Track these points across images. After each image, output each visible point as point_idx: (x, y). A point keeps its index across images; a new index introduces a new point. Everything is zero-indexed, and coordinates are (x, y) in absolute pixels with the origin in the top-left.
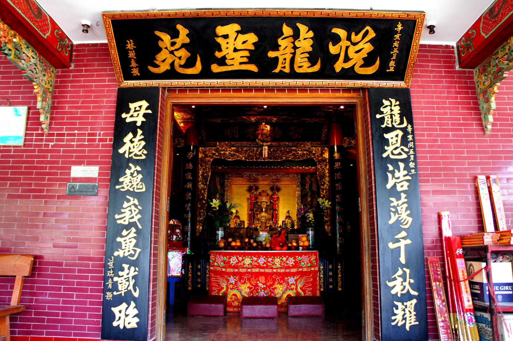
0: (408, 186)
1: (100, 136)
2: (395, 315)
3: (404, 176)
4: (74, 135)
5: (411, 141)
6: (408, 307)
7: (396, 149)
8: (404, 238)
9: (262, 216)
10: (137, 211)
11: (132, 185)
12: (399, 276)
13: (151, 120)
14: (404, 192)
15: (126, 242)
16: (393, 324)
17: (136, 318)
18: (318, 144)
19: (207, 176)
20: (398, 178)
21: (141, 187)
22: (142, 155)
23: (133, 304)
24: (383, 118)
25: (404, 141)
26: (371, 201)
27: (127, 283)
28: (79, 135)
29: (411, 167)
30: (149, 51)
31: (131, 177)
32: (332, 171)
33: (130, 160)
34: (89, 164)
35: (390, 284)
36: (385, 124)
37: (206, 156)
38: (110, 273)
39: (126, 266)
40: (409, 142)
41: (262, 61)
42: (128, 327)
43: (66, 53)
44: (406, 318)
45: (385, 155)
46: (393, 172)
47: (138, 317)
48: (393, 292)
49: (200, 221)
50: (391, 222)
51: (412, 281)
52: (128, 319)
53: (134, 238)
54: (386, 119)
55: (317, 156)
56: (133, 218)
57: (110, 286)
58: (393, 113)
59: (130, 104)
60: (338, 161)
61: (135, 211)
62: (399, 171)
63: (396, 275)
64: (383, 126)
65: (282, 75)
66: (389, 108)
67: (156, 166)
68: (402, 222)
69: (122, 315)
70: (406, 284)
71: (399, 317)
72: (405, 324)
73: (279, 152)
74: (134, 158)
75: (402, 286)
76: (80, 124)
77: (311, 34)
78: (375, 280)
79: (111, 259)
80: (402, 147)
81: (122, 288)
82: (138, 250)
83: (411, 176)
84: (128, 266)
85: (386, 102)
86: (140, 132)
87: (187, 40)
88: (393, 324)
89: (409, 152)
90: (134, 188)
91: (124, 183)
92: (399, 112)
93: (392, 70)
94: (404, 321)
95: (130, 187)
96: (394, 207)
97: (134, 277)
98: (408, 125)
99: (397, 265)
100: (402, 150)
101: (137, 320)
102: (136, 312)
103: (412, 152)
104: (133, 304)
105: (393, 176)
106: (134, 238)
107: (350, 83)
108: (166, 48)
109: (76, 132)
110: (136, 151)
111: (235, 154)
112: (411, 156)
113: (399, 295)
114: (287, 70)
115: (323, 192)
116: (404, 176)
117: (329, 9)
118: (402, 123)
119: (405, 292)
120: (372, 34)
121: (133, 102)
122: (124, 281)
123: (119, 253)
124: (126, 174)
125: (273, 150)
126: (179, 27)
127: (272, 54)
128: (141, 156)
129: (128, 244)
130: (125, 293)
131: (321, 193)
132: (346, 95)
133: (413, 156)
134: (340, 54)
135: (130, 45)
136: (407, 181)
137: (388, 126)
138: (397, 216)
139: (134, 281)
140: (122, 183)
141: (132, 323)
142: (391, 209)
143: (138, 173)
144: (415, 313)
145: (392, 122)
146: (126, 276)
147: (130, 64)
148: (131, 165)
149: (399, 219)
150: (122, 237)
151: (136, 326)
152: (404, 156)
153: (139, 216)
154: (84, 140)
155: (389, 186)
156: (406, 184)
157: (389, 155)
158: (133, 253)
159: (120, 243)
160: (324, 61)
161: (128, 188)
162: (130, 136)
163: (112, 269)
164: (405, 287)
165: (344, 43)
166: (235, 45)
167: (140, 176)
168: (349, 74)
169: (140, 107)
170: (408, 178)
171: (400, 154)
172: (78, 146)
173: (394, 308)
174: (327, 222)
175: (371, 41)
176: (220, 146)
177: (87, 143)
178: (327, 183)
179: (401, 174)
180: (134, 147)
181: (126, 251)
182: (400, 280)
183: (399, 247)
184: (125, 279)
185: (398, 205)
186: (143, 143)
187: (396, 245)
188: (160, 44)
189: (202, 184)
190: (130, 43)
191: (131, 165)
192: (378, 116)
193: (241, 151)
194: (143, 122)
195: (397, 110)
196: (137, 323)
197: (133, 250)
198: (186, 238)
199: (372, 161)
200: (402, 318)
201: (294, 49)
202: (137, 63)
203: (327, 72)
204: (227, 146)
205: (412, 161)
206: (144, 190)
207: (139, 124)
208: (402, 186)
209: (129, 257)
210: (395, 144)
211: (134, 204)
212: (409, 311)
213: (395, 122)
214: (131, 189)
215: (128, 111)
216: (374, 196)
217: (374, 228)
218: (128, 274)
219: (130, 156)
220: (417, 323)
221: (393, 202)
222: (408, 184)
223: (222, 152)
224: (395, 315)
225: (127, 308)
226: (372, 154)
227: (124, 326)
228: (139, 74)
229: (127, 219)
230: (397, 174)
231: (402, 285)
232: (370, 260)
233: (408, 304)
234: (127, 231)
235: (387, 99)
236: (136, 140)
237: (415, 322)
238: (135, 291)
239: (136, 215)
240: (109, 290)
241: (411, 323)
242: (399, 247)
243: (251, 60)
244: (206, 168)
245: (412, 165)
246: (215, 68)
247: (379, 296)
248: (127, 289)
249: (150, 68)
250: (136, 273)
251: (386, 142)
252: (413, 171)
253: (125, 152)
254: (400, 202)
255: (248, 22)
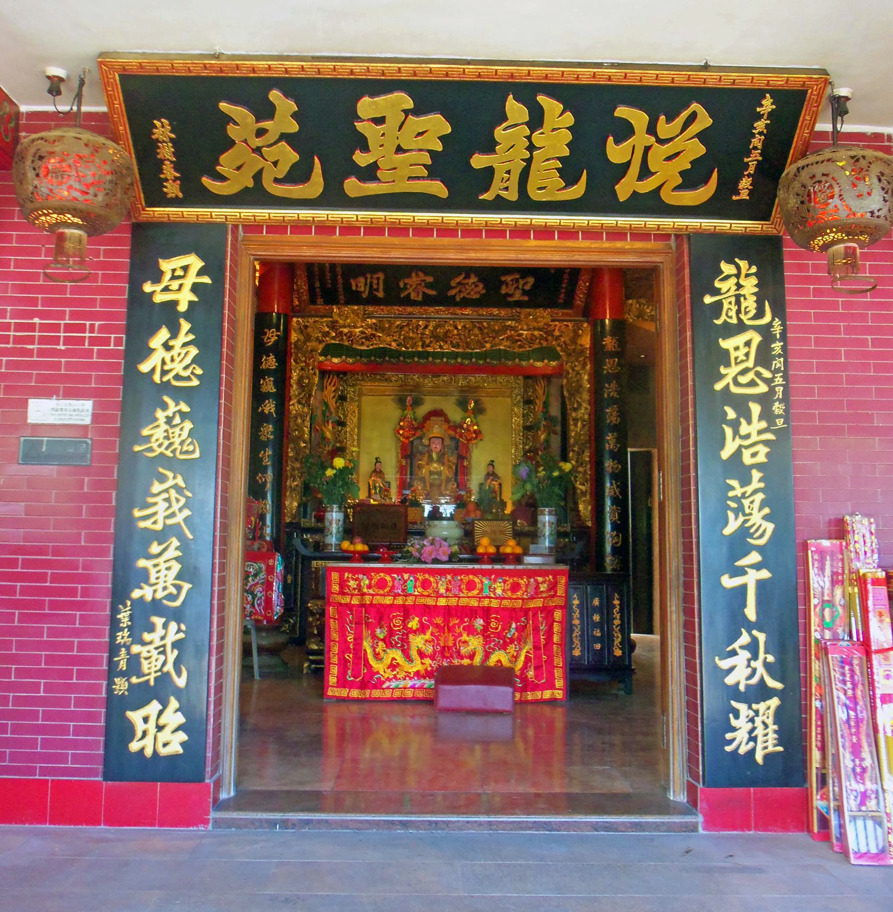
0: (768, 455)
1: (92, 330)
2: (734, 729)
3: (760, 432)
4: (32, 327)
5: (779, 356)
6: (761, 713)
7: (744, 372)
8: (757, 567)
9: (431, 473)
10: (183, 501)
11: (171, 444)
12: (742, 647)
13: (208, 298)
14: (759, 467)
15: (158, 568)
16: (728, 749)
17: (180, 732)
18: (568, 315)
19: (310, 384)
20: (748, 436)
21: (191, 448)
22: (193, 377)
23: (174, 704)
24: (719, 304)
25: (764, 357)
26: (685, 482)
27: (162, 658)
28: (43, 328)
29: (777, 412)
30: (203, 145)
31: (167, 427)
32: (598, 379)
33: (166, 387)
34: (70, 394)
35: (724, 664)
36: (723, 317)
37: (308, 338)
38: (122, 637)
39: (158, 621)
40: (773, 358)
41: (459, 178)
42: (163, 752)
43: (7, 136)
44: (756, 737)
45: (719, 386)
46: (735, 425)
47: (184, 731)
48: (730, 680)
49: (293, 490)
50: (727, 531)
51: (771, 658)
52: (163, 736)
53: (177, 559)
54: (726, 306)
55: (565, 342)
56: (173, 515)
57: (123, 665)
58: (742, 292)
59: (160, 261)
60: (612, 355)
61: (178, 500)
62: (749, 422)
63: (736, 645)
64: (718, 322)
65: (500, 205)
66: (733, 280)
67: (223, 401)
68: (752, 530)
69: (151, 726)
70: (758, 664)
71: (741, 736)
72: (752, 752)
73: (476, 331)
74: (175, 383)
75: (749, 670)
76: (46, 302)
77: (569, 119)
78: (690, 652)
79: (125, 606)
80: (759, 369)
81: (151, 668)
82: (186, 586)
83: (774, 432)
84: (164, 620)
85: (727, 268)
86: (185, 326)
87: (294, 127)
88: (728, 749)
89: (772, 380)
90: (174, 451)
91: (153, 439)
92: (756, 290)
93: (744, 195)
94: (751, 744)
95: (167, 449)
96: (736, 499)
97: (176, 645)
98: (773, 319)
99: (737, 623)
100: (758, 374)
101: (182, 736)
102: (180, 719)
103: (779, 380)
104: (174, 704)
105: (736, 433)
106: (177, 559)
107: (652, 222)
108: (245, 141)
109: (36, 320)
110: (178, 368)
111: (374, 335)
112: (777, 389)
113: (742, 688)
114: (512, 195)
115: (576, 425)
116: (760, 432)
117: (613, 66)
118: (760, 314)
119: (754, 681)
120: (704, 121)
121: (169, 256)
122: (154, 653)
123: (144, 593)
124: (156, 419)
125: (464, 326)
126: (275, 95)
127: (479, 161)
128: (188, 379)
129: (164, 572)
130: (156, 679)
131: (572, 427)
132: (639, 245)
133: (782, 388)
134: (629, 162)
135: (162, 130)
136: (766, 443)
137: (729, 320)
138: (741, 518)
139: (176, 652)
140: (148, 438)
141: (174, 743)
142: (729, 502)
143: (184, 416)
144: (776, 727)
145: (738, 312)
146: (158, 643)
147: (161, 171)
148: (166, 399)
149: (746, 525)
150: (149, 557)
151: (181, 751)
152: (763, 388)
153: (187, 513)
154: (56, 340)
155: (725, 454)
156: (763, 450)
157: (728, 384)
158: (174, 591)
159: (145, 571)
160: (592, 175)
161: (162, 449)
162: (163, 334)
163: (128, 626)
164: (754, 671)
165: (641, 138)
166: (400, 141)
167: (188, 425)
168: (650, 204)
169: (185, 268)
170: (770, 436)
171: (752, 384)
172: (41, 353)
173: (731, 716)
174: (584, 494)
175: (702, 136)
176: (340, 315)
177: (63, 348)
178: (585, 405)
179: (753, 427)
180: (172, 360)
181: (159, 587)
182: (745, 655)
183: (744, 588)
184: (156, 648)
185: (743, 495)
186: (194, 351)
187: (737, 581)
188: (232, 131)
189: (299, 402)
190: (163, 126)
191: (166, 399)
192: (708, 300)
193: (390, 327)
194: (191, 303)
195: (750, 286)
196: (183, 744)
197: (173, 585)
198: (262, 529)
199: (690, 397)
200: (747, 736)
201: (531, 146)
202: (176, 170)
203: (600, 200)
204: (357, 315)
205: (778, 399)
206: (197, 455)
207: (183, 307)
208: (754, 455)
209: (165, 602)
210: (742, 361)
211: (176, 487)
212: (764, 723)
213: (746, 313)
214: (169, 453)
215: (157, 277)
216: (692, 474)
217: (691, 542)
218: (163, 638)
219: (165, 379)
220: (780, 749)
221: (733, 488)
222: (767, 450)
223: (346, 330)
224: (734, 729)
225: (161, 713)
226: (690, 383)
227: (155, 752)
228: (181, 195)
229: (160, 517)
230: (744, 429)
231: (749, 666)
232: (681, 608)
233: (761, 707)
234: (160, 544)
235: (730, 261)
236: (177, 343)
237: (775, 746)
238: (179, 674)
239: (180, 510)
240: (123, 674)
241: (766, 748)
242: (744, 588)
243: (433, 172)
244: (308, 365)
245: (778, 408)
246: (353, 186)
247: (699, 688)
248: (160, 670)
249: (206, 181)
250: (181, 635)
251: (724, 358)
252: (780, 422)
253: (153, 370)
254: (749, 489)
255: (430, 92)
